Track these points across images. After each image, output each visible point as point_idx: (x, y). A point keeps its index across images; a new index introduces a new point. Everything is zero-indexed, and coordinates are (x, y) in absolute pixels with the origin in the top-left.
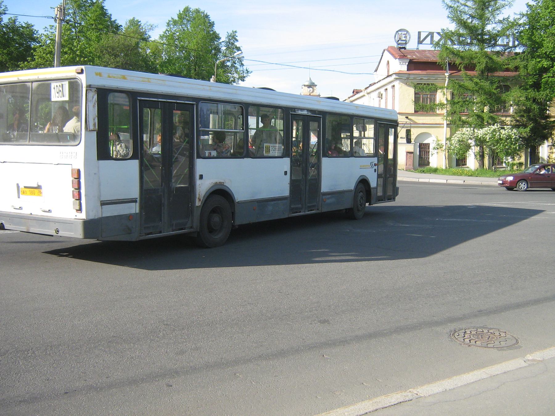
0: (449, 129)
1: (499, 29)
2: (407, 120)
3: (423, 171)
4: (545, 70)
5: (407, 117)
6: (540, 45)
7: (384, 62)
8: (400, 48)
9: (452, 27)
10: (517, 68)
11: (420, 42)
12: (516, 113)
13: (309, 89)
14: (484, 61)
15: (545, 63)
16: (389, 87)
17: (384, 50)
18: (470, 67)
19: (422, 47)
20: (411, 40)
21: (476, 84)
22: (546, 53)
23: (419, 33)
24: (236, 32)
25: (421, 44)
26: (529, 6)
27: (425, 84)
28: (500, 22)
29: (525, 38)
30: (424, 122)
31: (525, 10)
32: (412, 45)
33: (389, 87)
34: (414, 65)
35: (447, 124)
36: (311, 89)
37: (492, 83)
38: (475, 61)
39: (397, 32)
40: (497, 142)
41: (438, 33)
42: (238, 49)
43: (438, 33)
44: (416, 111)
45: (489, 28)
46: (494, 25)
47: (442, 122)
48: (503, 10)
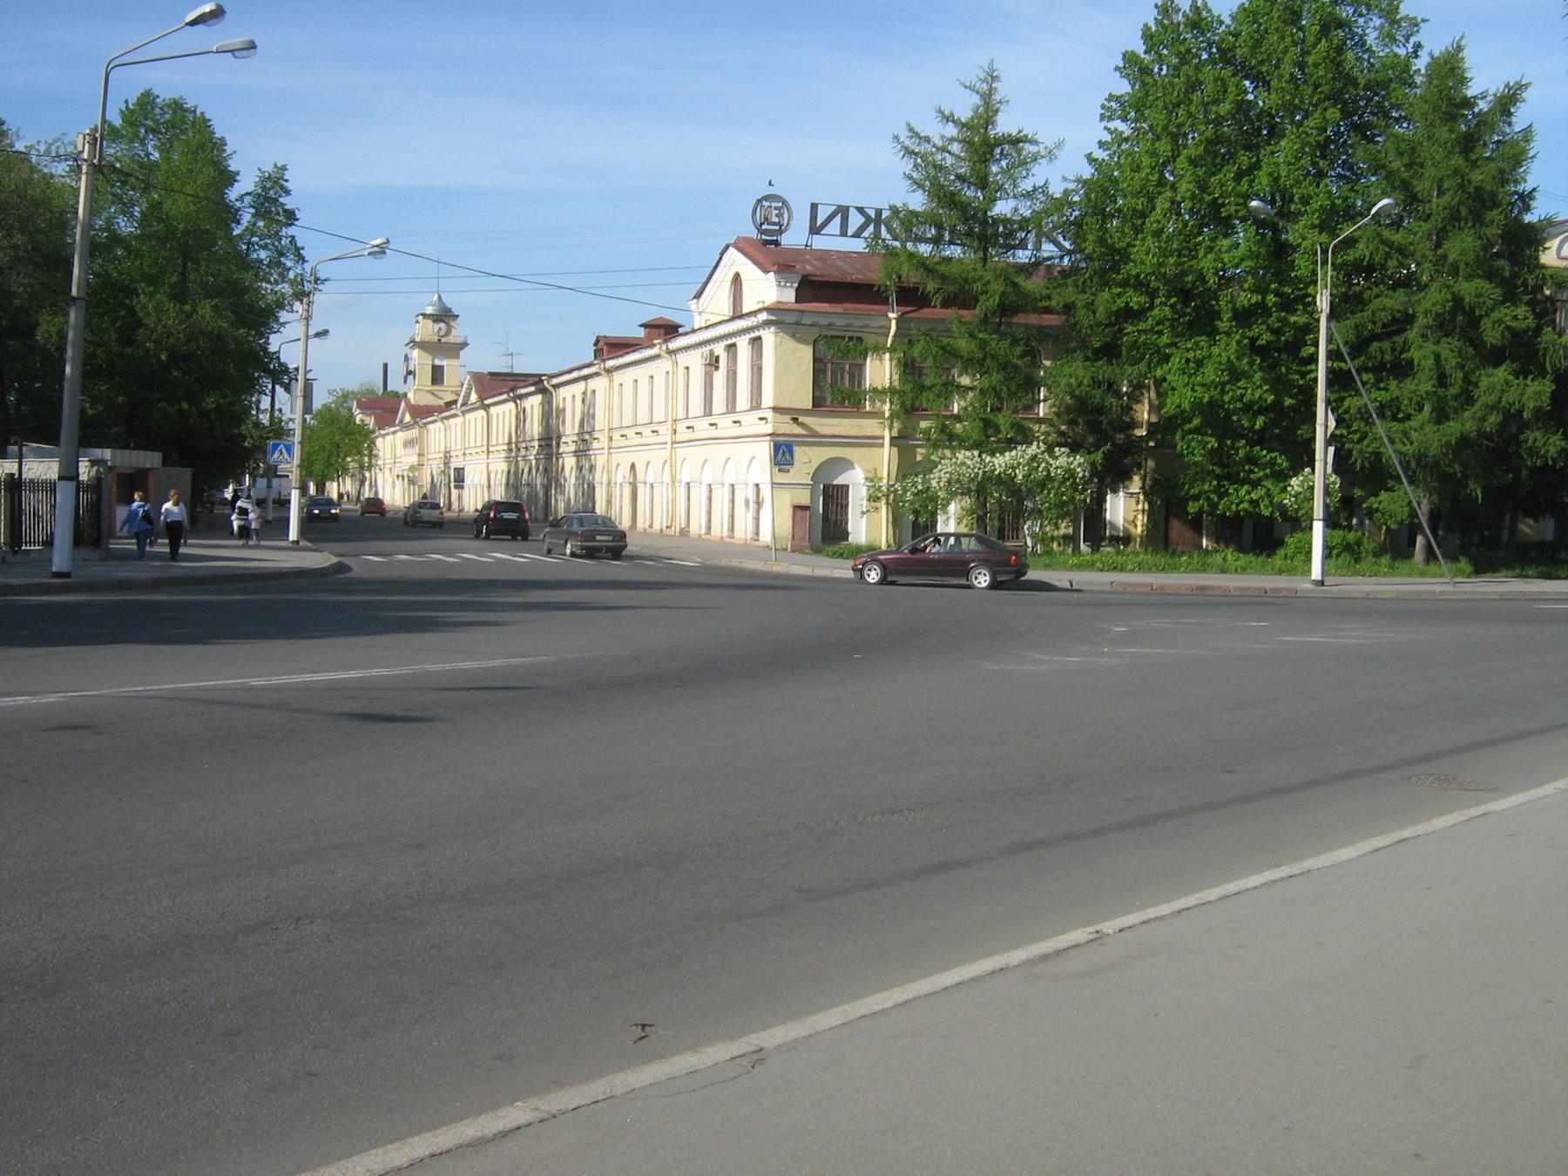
0: (895, 450)
1: (1027, 213)
2: (798, 430)
3: (841, 555)
4: (1128, 314)
5: (795, 420)
6: (1124, 256)
7: (723, 277)
8: (766, 243)
9: (917, 201)
10: (1069, 309)
11: (815, 230)
12: (1058, 414)
13: (437, 327)
14: (997, 287)
15: (1136, 300)
16: (743, 344)
17: (727, 247)
18: (961, 297)
19: (819, 243)
20: (792, 224)
21: (983, 344)
22: (1138, 275)
23: (814, 207)
24: (284, 168)
25: (818, 233)
26: (1091, 159)
27: (851, 338)
28: (1028, 195)
29: (1091, 238)
30: (837, 433)
31: (1087, 172)
32: (795, 237)
33: (743, 344)
34: (819, 286)
35: (892, 439)
36: (442, 325)
37: (1015, 342)
38: (977, 286)
39: (760, 201)
40: (1042, 485)
41: (861, 210)
42: (291, 217)
43: (861, 210)
44: (818, 403)
45: (1002, 208)
46: (1012, 203)
47: (878, 432)
48: (1036, 169)
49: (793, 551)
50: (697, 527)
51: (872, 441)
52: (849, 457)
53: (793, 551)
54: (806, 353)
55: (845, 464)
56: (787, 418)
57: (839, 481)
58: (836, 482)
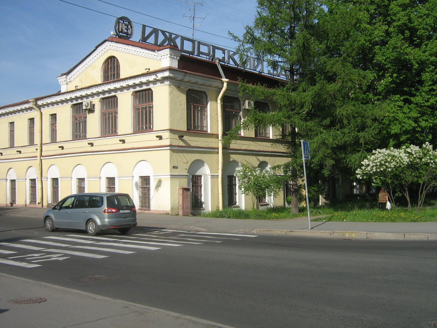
2: (181, 144)
23: (144, 27)
41: (163, 32)
43: (163, 32)
49: (184, 215)
50: (23, 198)
51: (213, 150)
52: (236, 159)
53: (184, 215)
54: (183, 98)
55: (198, 164)
56: (177, 136)
57: (198, 174)
58: (196, 174)
